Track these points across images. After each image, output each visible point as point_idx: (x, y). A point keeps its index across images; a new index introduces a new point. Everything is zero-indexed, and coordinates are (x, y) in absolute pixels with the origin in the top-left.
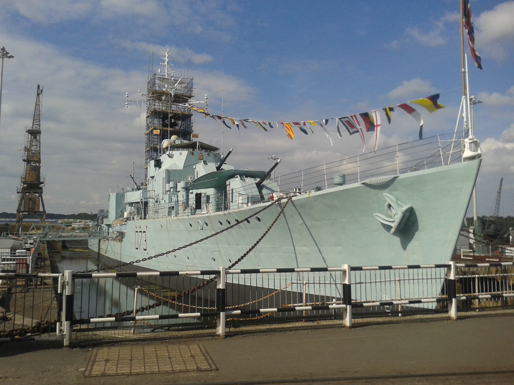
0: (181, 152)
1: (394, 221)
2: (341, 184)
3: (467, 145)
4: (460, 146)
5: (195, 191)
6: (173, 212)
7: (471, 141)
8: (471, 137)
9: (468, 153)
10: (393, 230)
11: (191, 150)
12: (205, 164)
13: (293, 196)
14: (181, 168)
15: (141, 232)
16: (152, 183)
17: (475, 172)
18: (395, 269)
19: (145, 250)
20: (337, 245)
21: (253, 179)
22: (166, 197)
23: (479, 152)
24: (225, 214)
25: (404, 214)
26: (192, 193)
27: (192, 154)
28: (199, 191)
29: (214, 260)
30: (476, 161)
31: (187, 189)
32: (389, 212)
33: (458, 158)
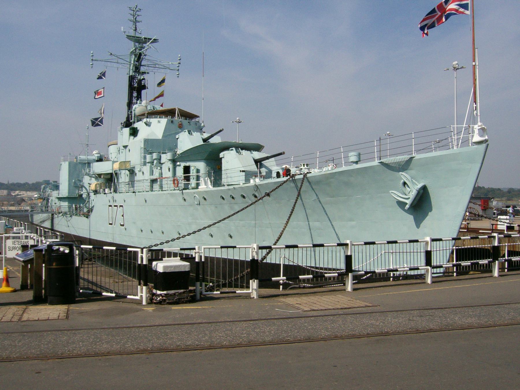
0: (160, 119)
1: (409, 198)
2: (356, 163)
3: (476, 131)
4: (469, 131)
5: (183, 164)
6: (156, 186)
7: (480, 127)
8: (479, 124)
9: (477, 138)
10: (407, 206)
11: (169, 117)
12: (189, 133)
13: (308, 173)
14: (161, 138)
15: (115, 206)
16: (124, 153)
17: (483, 155)
18: (378, 244)
19: (123, 225)
20: (351, 220)
21: (249, 152)
22: (147, 169)
23: (486, 138)
24: (229, 189)
25: (419, 192)
26: (180, 165)
27: (172, 122)
28: (187, 164)
29: (212, 236)
30: (484, 145)
31: (174, 161)
32: (403, 189)
33: (465, 142)
